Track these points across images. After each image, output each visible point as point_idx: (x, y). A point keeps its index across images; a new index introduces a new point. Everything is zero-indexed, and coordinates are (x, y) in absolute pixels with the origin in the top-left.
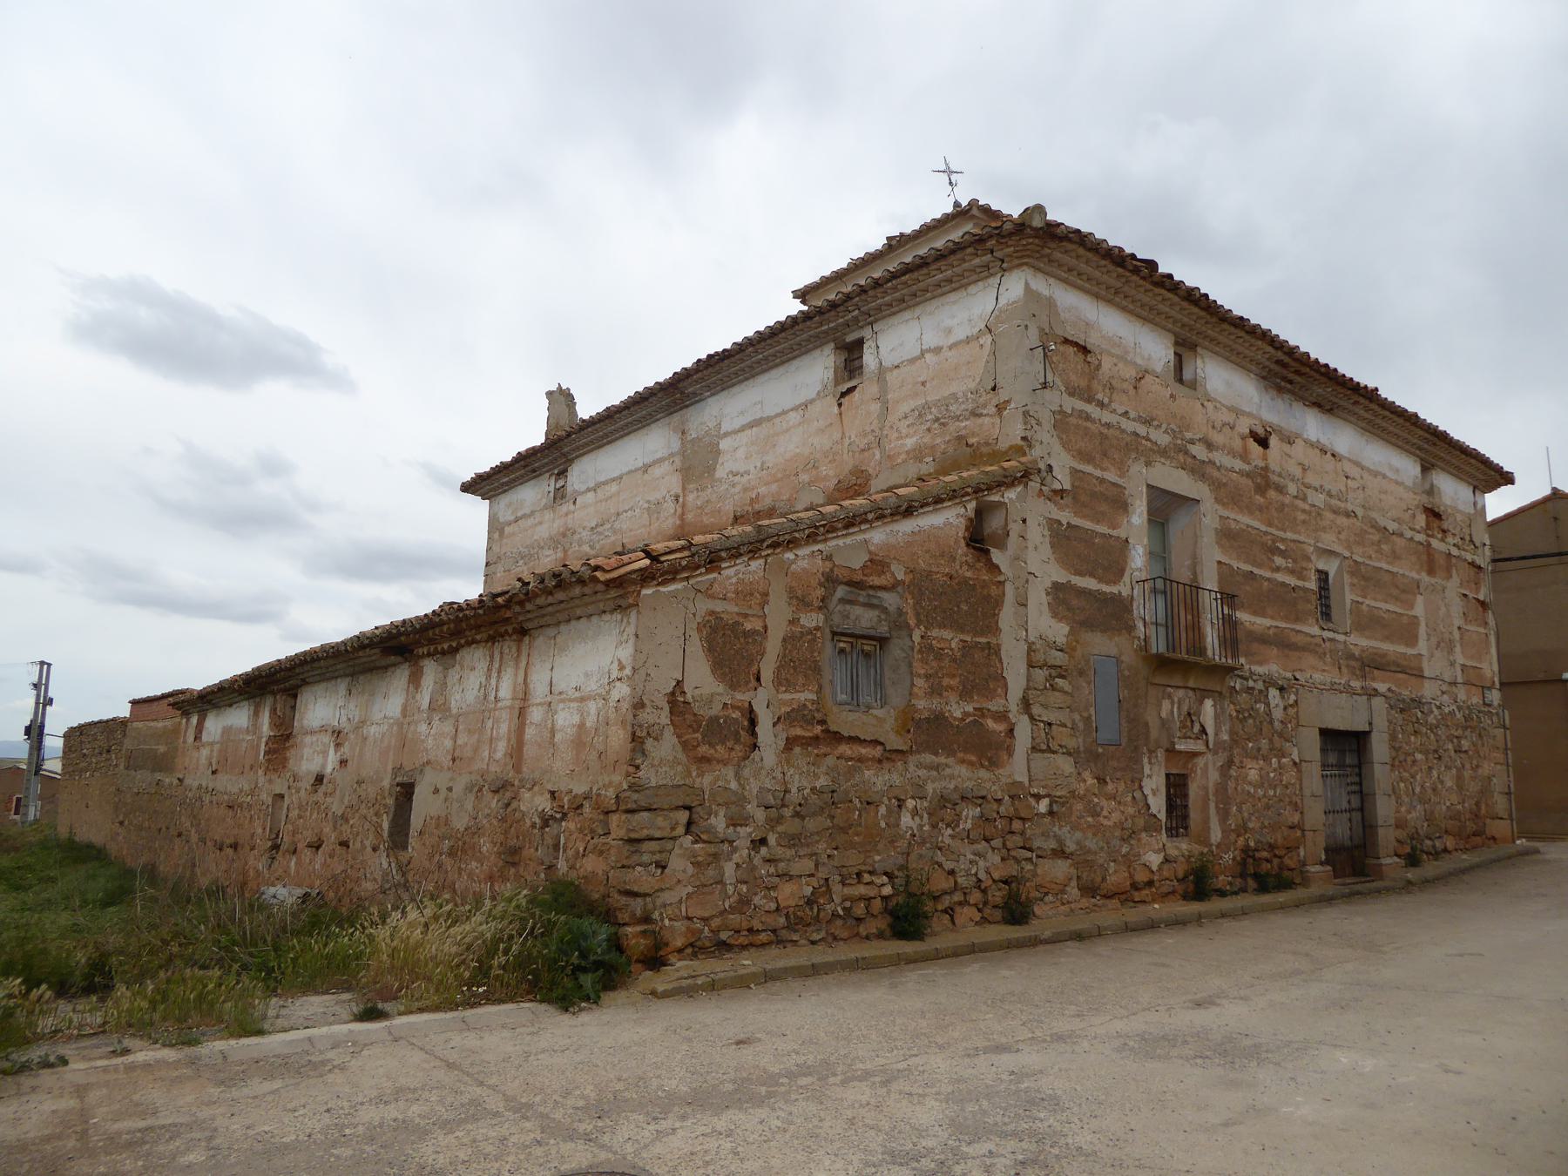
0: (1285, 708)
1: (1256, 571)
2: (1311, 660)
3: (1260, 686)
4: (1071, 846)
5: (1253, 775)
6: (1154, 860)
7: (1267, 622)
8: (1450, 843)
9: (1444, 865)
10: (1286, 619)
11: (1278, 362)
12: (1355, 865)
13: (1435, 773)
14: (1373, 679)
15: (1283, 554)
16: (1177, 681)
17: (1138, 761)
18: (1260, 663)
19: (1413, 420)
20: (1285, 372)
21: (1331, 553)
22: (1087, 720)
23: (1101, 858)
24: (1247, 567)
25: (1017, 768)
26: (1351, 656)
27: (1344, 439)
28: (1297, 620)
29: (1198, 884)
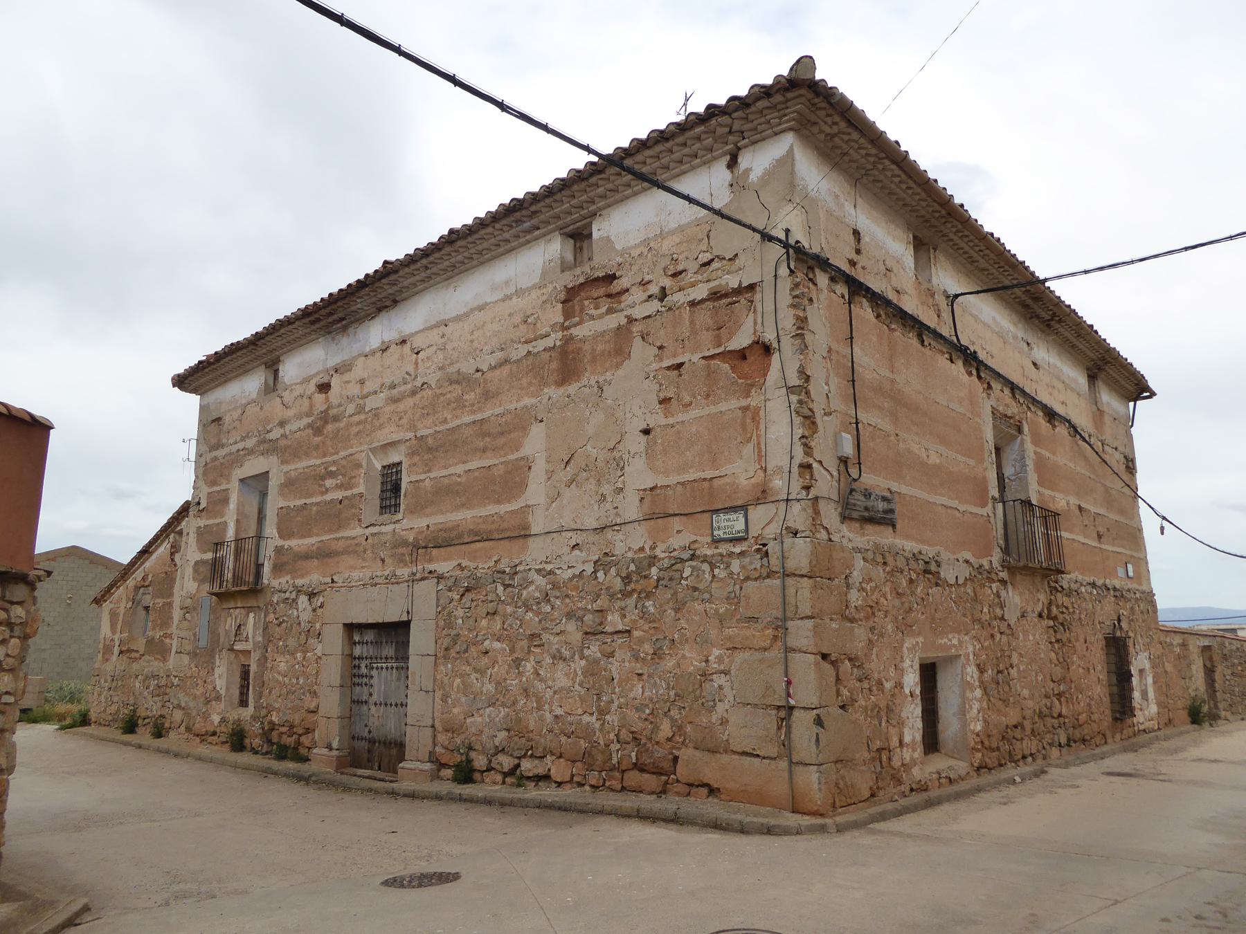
0: (314, 610)
1: (308, 501)
2: (349, 560)
3: (294, 595)
4: (183, 705)
5: (283, 667)
6: (216, 719)
7: (313, 540)
8: (558, 770)
9: (546, 793)
10: (330, 531)
11: (313, 323)
12: (372, 758)
13: (529, 667)
14: (430, 561)
15: (332, 475)
16: (232, 605)
17: (214, 657)
18: (302, 576)
19: (454, 237)
20: (322, 323)
21: (392, 444)
22: (195, 635)
23: (194, 713)
24: (299, 502)
25: (172, 660)
26: (404, 543)
27: (414, 317)
28: (339, 528)
29: (238, 741)
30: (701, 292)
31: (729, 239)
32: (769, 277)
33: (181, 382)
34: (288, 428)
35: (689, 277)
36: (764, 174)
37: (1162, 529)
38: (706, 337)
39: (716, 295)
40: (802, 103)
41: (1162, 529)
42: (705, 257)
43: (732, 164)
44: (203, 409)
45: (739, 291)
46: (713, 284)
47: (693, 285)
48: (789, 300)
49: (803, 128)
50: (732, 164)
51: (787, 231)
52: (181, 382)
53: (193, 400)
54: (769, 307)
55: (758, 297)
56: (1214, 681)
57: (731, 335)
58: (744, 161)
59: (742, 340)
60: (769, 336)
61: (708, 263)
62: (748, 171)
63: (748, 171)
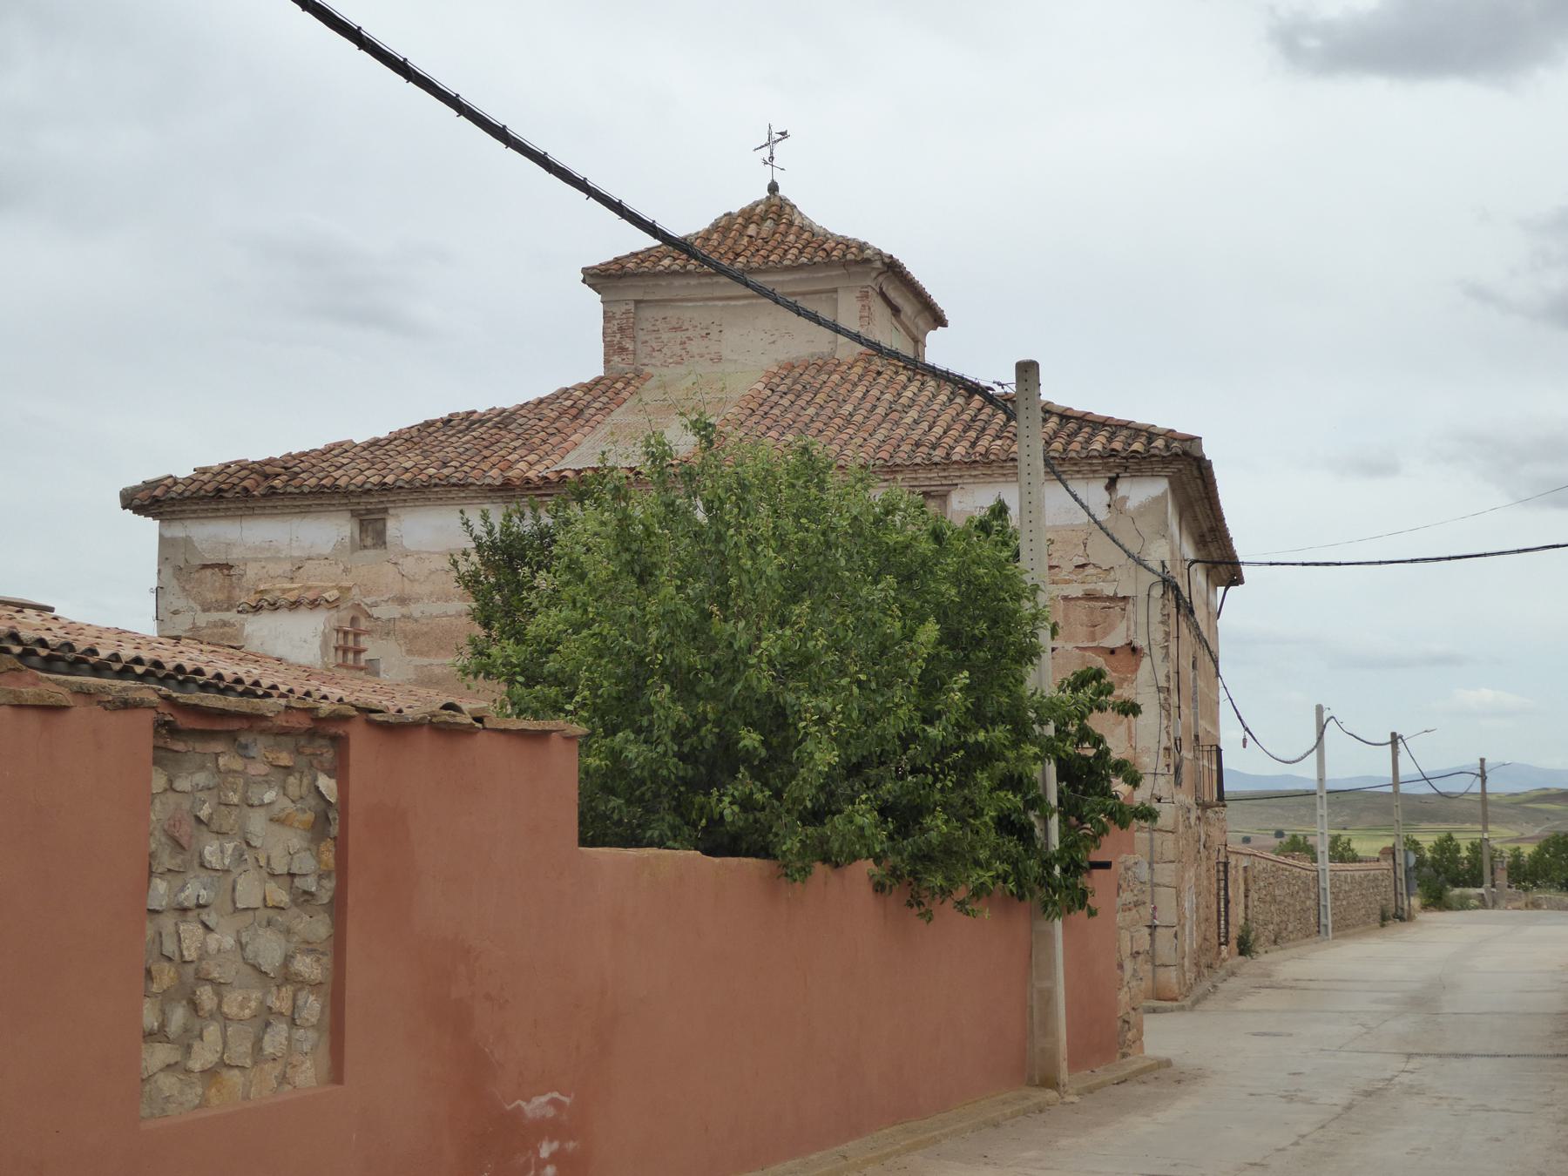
30: (1076, 590)
31: (1102, 552)
32: (1143, 595)
33: (149, 500)
34: (415, 610)
35: (1063, 575)
36: (1140, 506)
37: (1245, 741)
38: (1082, 631)
39: (1090, 597)
40: (1185, 469)
41: (1245, 741)
42: (1082, 561)
43: (1111, 485)
44: (163, 540)
45: (1114, 598)
46: (1087, 587)
47: (1067, 582)
48: (1159, 618)
49: (1177, 487)
50: (1111, 485)
51: (1027, 371)
52: (149, 500)
53: (149, 527)
54: (1142, 619)
55: (1130, 607)
56: (1197, 627)
57: (1105, 634)
58: (1123, 488)
59: (1116, 640)
60: (1141, 642)
61: (1083, 566)
62: (1125, 499)
63: (1125, 499)
